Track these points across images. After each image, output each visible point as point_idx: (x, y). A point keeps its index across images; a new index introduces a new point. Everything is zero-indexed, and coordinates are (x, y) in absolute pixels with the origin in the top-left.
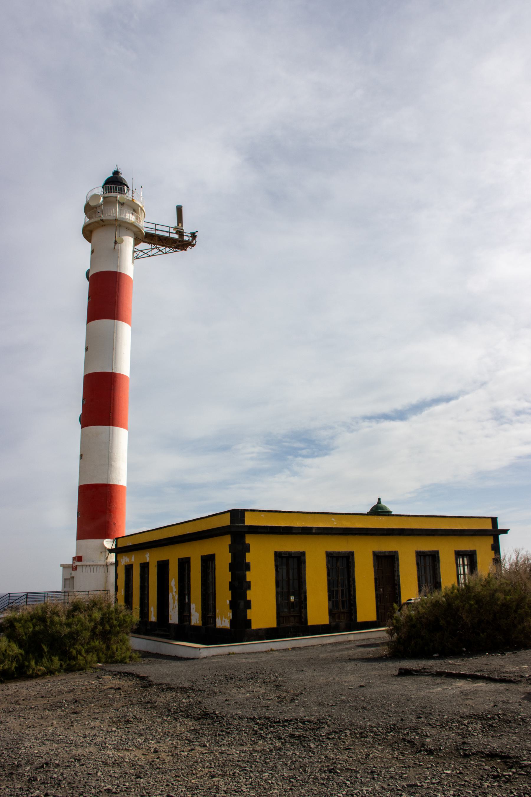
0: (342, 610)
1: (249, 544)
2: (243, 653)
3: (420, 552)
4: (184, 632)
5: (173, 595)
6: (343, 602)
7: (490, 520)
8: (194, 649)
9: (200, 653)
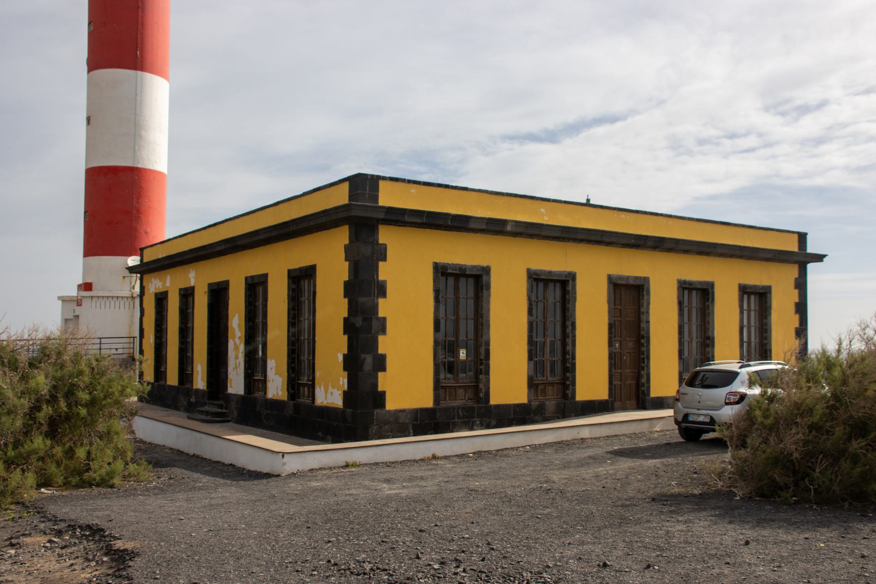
0: (550, 379)
1: (385, 245)
2: (377, 464)
3: (685, 282)
4: (255, 413)
5: (235, 344)
6: (553, 364)
7: (796, 235)
8: (269, 454)
9: (284, 464)
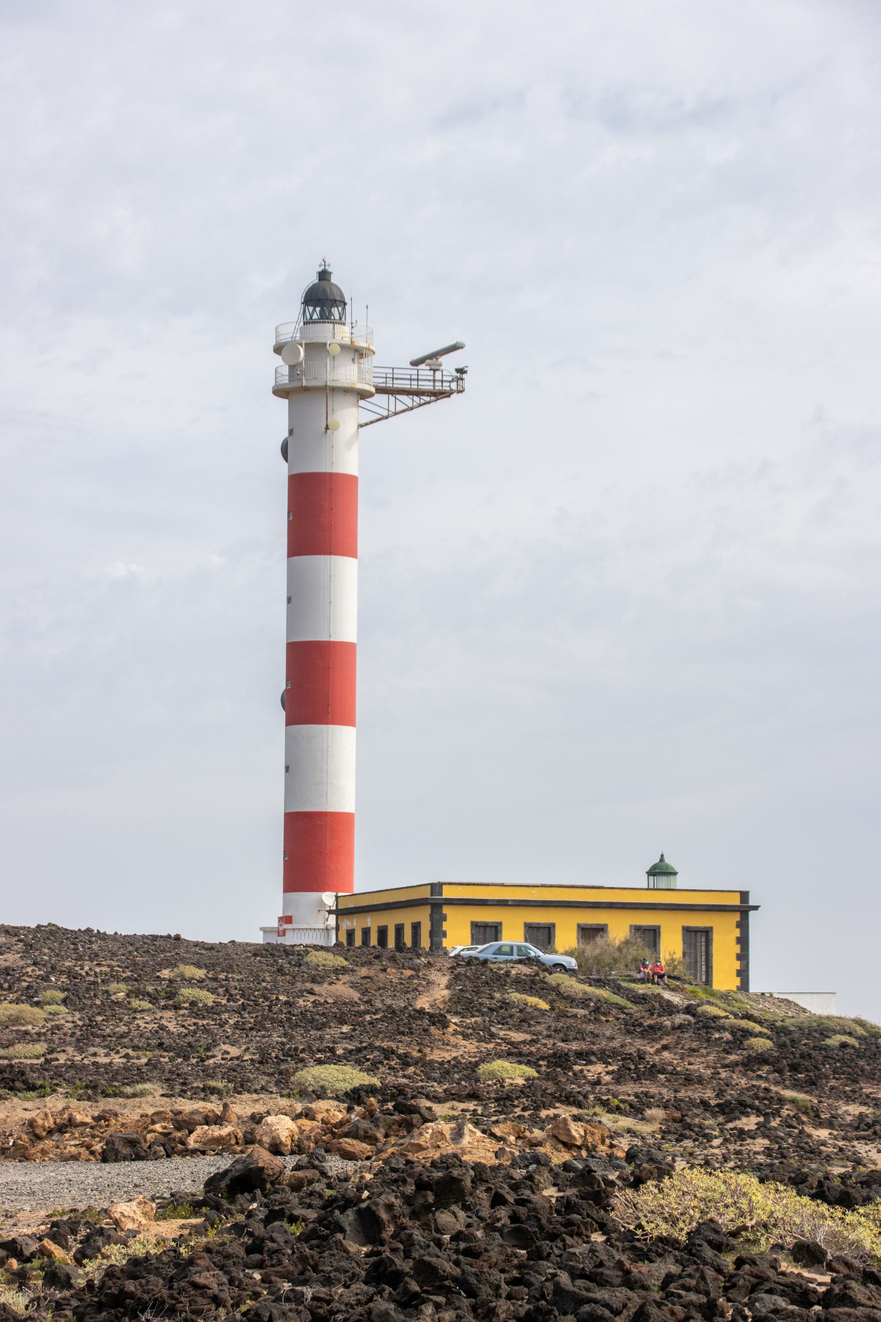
3: (529, 924)
